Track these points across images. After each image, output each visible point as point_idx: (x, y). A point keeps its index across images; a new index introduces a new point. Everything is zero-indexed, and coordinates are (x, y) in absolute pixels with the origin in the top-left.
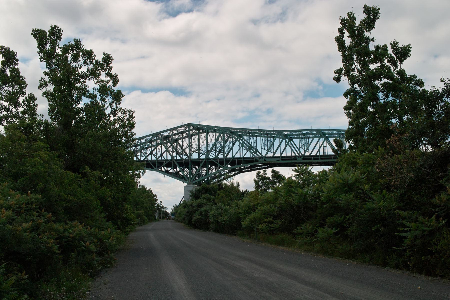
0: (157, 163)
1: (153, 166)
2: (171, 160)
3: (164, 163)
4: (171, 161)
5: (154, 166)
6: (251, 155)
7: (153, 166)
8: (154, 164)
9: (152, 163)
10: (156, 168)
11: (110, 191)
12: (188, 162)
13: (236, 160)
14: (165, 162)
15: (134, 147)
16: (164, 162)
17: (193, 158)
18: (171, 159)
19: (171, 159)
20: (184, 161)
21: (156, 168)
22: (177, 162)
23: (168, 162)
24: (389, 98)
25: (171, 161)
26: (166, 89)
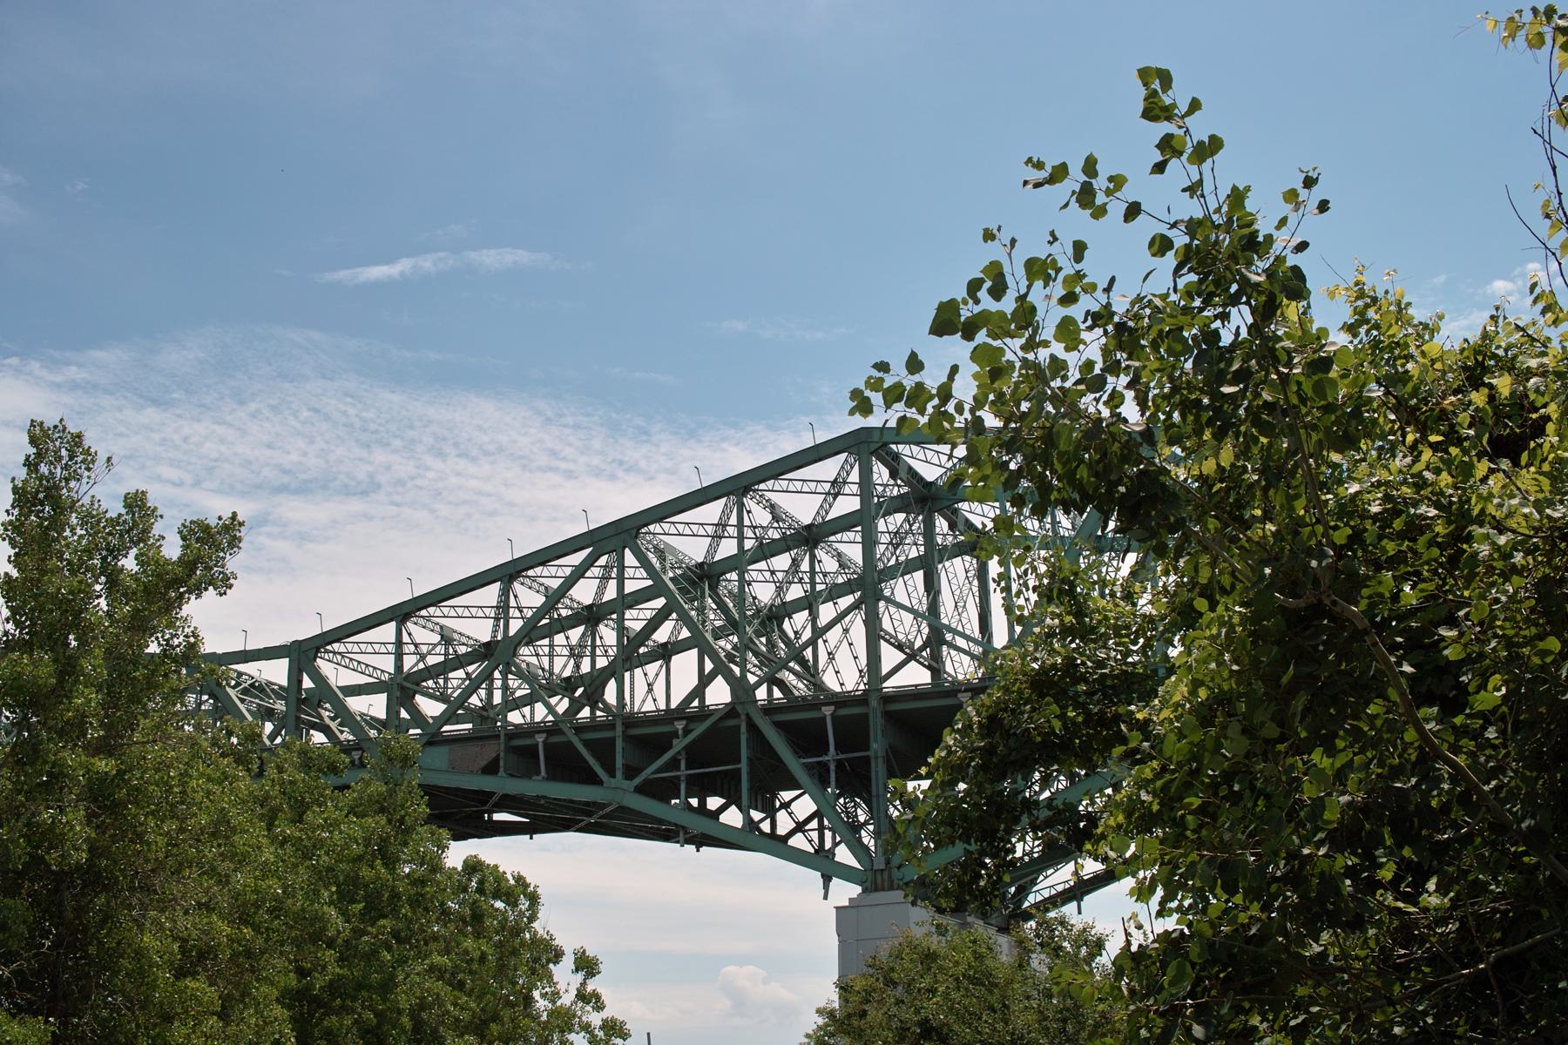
0: (628, 739)
1: (592, 761)
2: (730, 711)
3: (675, 734)
4: (731, 723)
5: (603, 766)
6: (719, 694)
7: (592, 761)
8: (604, 750)
9: (586, 743)
10: (619, 774)
11: (1293, 767)
12: (866, 716)
13: (540, 738)
14: (687, 732)
15: (581, 629)
16: (680, 725)
17: (930, 681)
18: (728, 700)
19: (728, 700)
20: (828, 711)
21: (619, 774)
22: (779, 725)
23: (700, 729)
24: (1085, 182)
25: (731, 723)
26: (1201, 174)
